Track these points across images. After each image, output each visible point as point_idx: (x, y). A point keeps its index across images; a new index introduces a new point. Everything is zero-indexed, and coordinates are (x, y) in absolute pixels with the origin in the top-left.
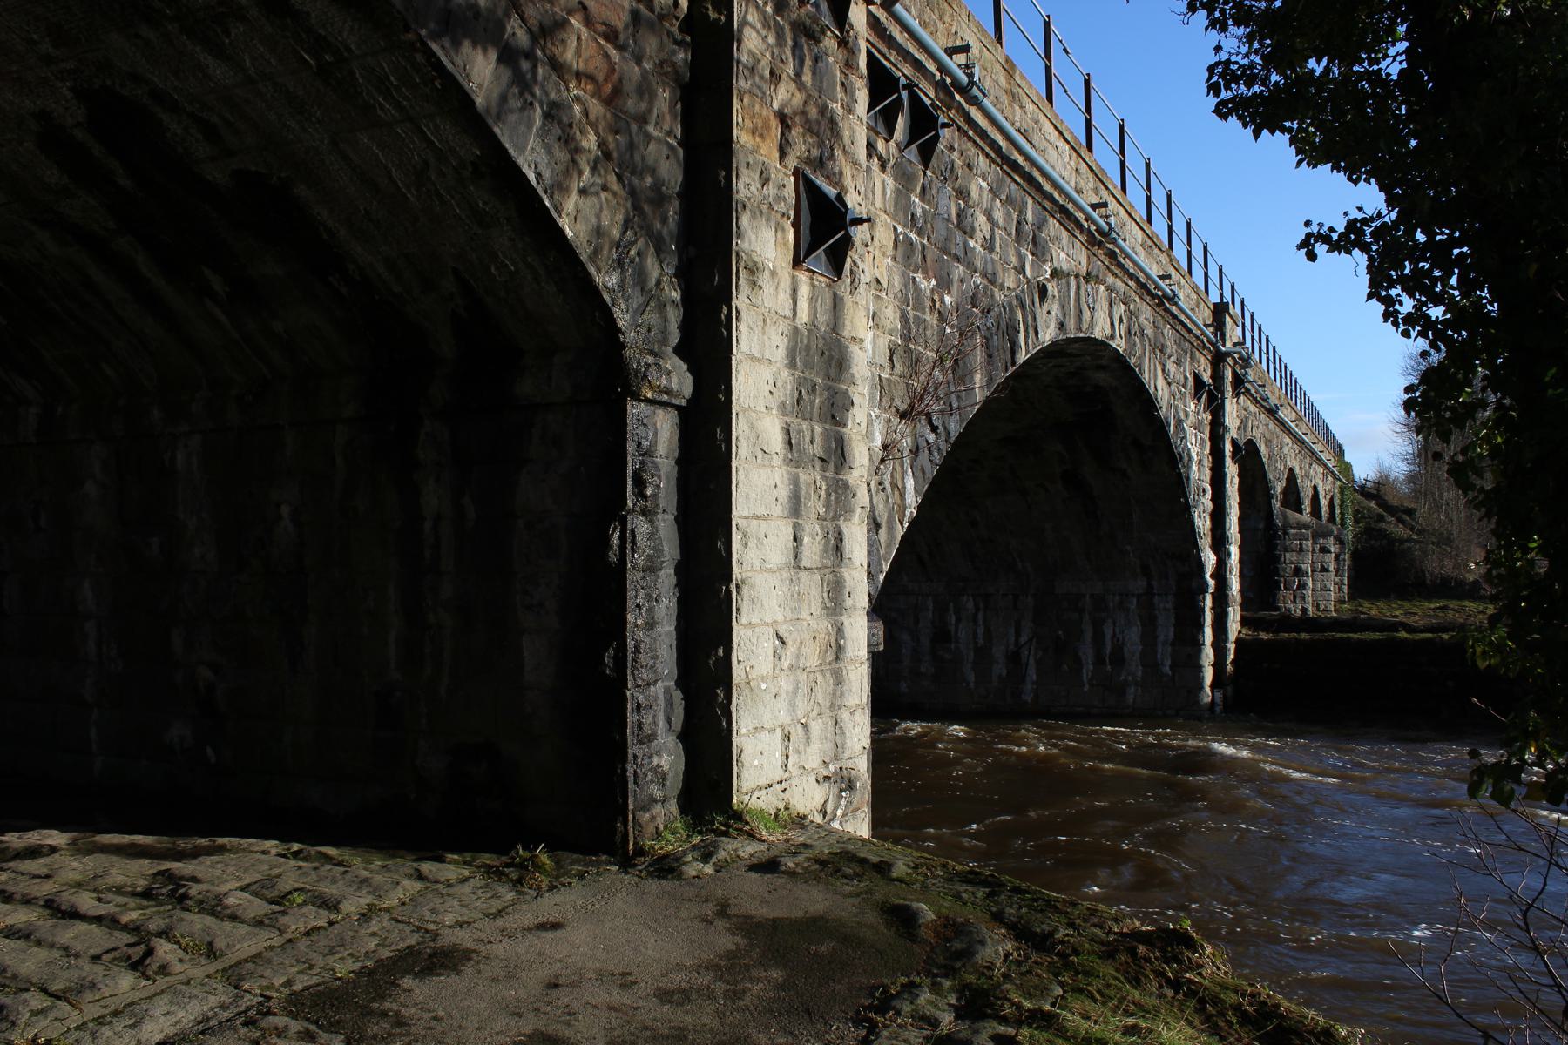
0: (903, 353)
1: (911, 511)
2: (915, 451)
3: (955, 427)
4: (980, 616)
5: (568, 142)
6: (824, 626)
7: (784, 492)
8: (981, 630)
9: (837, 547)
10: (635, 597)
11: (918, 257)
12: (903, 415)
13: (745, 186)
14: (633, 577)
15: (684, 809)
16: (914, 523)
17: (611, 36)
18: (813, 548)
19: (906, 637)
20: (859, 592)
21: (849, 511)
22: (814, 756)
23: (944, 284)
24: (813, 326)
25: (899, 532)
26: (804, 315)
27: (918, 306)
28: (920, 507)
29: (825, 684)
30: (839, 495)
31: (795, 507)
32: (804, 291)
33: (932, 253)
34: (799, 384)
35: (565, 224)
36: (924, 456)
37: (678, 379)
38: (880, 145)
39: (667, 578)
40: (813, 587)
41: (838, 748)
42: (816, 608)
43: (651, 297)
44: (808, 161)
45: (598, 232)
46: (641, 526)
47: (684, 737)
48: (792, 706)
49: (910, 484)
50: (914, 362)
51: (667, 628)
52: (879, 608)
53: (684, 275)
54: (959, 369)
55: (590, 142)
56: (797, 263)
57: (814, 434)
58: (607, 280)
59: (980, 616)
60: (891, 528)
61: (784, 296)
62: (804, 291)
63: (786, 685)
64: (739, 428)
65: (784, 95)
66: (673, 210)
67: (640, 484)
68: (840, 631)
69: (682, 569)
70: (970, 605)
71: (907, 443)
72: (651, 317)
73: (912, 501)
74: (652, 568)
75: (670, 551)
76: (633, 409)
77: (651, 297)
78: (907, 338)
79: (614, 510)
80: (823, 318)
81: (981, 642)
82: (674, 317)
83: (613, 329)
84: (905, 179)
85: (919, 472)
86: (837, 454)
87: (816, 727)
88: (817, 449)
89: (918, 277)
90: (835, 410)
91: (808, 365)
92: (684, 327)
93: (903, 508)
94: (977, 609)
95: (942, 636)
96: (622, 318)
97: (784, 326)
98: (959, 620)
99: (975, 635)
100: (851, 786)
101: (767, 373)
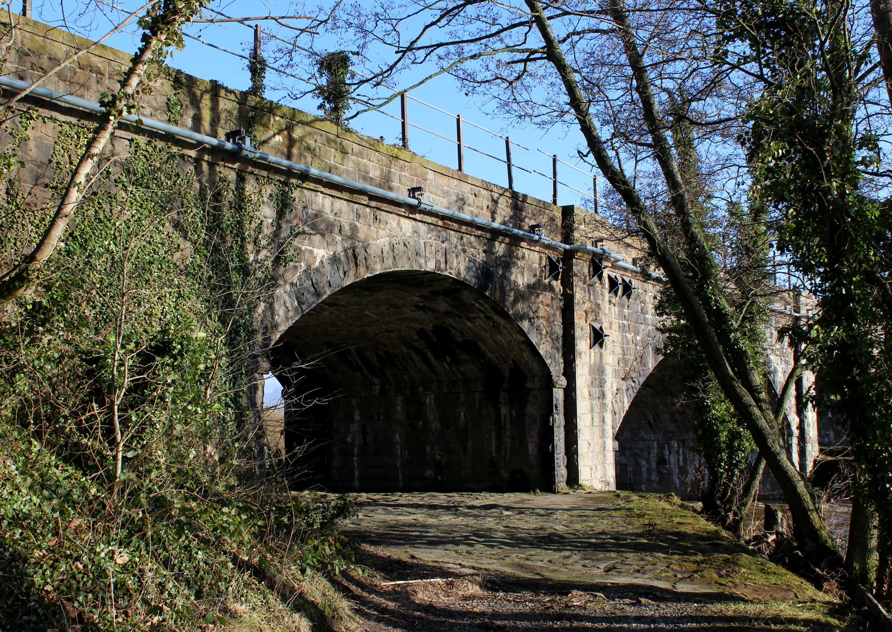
0: (623, 360)
1: (627, 408)
2: (628, 390)
3: (642, 380)
4: (681, 450)
5: (541, 334)
6: (600, 441)
7: (589, 407)
8: (681, 458)
9: (603, 420)
10: (556, 433)
11: (627, 328)
12: (623, 379)
13: (578, 333)
14: (555, 429)
15: (567, 484)
16: (627, 412)
17: (548, 305)
18: (597, 421)
19: (644, 462)
20: (610, 433)
21: (606, 411)
22: (599, 475)
23: (637, 333)
24: (595, 362)
25: (623, 415)
26: (593, 361)
27: (628, 343)
28: (630, 407)
29: (601, 457)
30: (603, 406)
31: (592, 411)
32: (593, 355)
33: (632, 325)
34: (592, 378)
35: (541, 352)
36: (631, 391)
37: (563, 382)
38: (613, 301)
39: (562, 429)
40: (597, 431)
41: (605, 475)
42: (598, 436)
43: (557, 363)
44: (593, 320)
45: (547, 351)
46: (556, 416)
47: (567, 467)
48: (592, 461)
49: (626, 400)
50: (626, 361)
51: (563, 441)
52: (617, 437)
53: (564, 356)
54: (642, 359)
55: (544, 332)
56: (590, 348)
57: (596, 391)
58: (548, 362)
59: (681, 450)
60: (620, 414)
61: (588, 357)
62: (593, 355)
63: (591, 455)
64: (578, 393)
65: (587, 305)
66: (561, 340)
67: (556, 407)
68: (604, 443)
69: (565, 427)
70: (676, 445)
71: (624, 388)
72: (557, 368)
73: (627, 405)
74: (559, 427)
75: (563, 423)
76: (554, 390)
77: (557, 363)
78: (624, 355)
79: (550, 413)
80: (598, 360)
81: (682, 464)
82: (562, 366)
83: (550, 372)
84: (622, 306)
85: (629, 396)
86: (603, 395)
87: (599, 467)
88: (597, 395)
89: (627, 334)
90: (602, 384)
91: (594, 374)
92: (564, 369)
93: (623, 408)
94: (679, 448)
95: (662, 461)
96: (551, 369)
97: (588, 365)
98: (670, 453)
99: (679, 460)
100: (609, 484)
101: (584, 378)
